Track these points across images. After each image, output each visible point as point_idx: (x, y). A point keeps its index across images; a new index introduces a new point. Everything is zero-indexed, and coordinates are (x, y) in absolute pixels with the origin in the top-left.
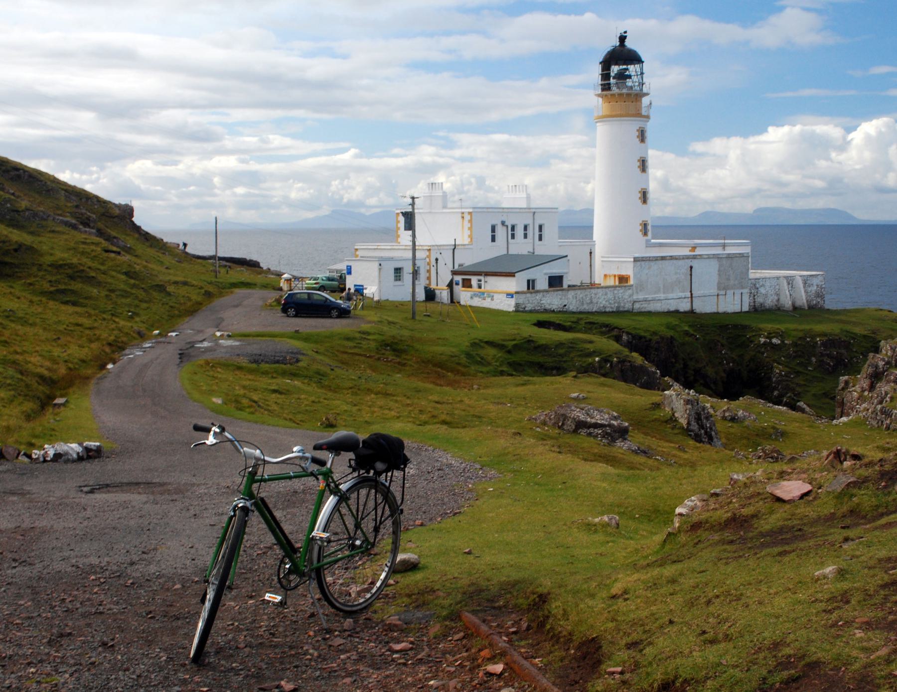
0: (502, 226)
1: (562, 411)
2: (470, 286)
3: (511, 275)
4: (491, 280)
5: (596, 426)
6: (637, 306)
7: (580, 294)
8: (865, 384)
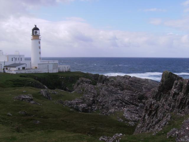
0: (14, 58)
1: (19, 96)
2: (7, 69)
3: (15, 67)
4: (11, 68)
5: (26, 99)
6: (39, 72)
7: (28, 70)
8: (77, 85)
